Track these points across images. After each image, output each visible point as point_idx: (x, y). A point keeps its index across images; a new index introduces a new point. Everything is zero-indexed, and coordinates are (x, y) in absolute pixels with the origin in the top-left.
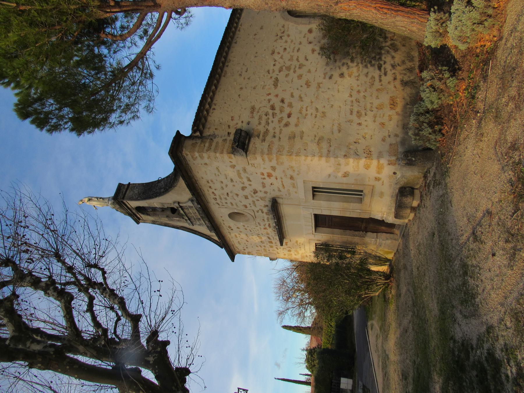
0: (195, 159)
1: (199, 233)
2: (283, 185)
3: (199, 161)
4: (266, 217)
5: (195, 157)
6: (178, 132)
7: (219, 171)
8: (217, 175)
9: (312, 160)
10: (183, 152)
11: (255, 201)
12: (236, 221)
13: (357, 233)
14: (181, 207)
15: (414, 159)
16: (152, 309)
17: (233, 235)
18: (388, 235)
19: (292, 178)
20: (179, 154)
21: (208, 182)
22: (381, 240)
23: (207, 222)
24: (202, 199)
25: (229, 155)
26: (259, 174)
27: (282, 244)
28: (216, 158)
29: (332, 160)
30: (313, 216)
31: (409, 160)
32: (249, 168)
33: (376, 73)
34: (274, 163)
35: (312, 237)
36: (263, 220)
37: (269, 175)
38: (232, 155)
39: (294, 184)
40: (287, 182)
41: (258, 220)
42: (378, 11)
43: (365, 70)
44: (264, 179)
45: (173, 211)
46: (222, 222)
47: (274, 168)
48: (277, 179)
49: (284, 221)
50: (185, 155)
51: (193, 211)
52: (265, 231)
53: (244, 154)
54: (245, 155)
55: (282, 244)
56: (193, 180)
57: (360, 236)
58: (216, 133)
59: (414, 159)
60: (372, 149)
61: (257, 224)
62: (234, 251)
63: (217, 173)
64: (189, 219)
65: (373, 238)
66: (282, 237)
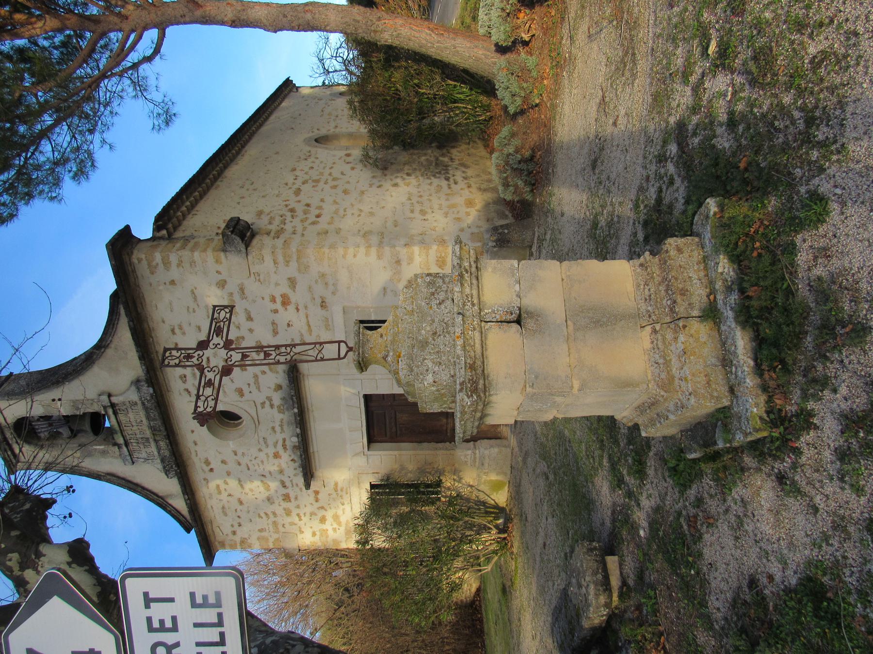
0: (153, 270)
1: (143, 488)
2: (309, 326)
3: (162, 275)
4: (278, 417)
5: (154, 263)
6: (127, 228)
7: (195, 299)
8: (191, 310)
9: (355, 256)
10: (134, 256)
11: (259, 374)
12: (221, 439)
13: (440, 445)
14: (113, 405)
15: (506, 231)
16: (36, 460)
17: (213, 485)
18: (493, 441)
19: (323, 305)
20: (126, 258)
21: (173, 331)
22: (482, 450)
23: (162, 444)
24: (157, 379)
25: (216, 253)
26: (267, 299)
27: (308, 486)
28: (193, 263)
29: (387, 250)
30: (362, 400)
31: (500, 234)
32: (252, 287)
33: (444, 183)
34: (292, 270)
35: (361, 461)
36: (273, 428)
37: (286, 302)
38: (222, 254)
39: (327, 319)
40: (316, 312)
41: (264, 431)
42: (432, 31)
43: (429, 181)
44: (276, 311)
45: (96, 421)
46: (191, 445)
47: (292, 282)
48: (298, 310)
49: (312, 424)
50: (136, 261)
51: (136, 421)
52: (276, 461)
53: (242, 247)
54: (244, 250)
55: (308, 486)
56: (146, 326)
57: (447, 449)
58: (195, 234)
59: (506, 231)
60: (446, 238)
61: (261, 440)
62: (212, 538)
63: (192, 305)
64: (127, 444)
65: (469, 449)
66: (308, 474)
